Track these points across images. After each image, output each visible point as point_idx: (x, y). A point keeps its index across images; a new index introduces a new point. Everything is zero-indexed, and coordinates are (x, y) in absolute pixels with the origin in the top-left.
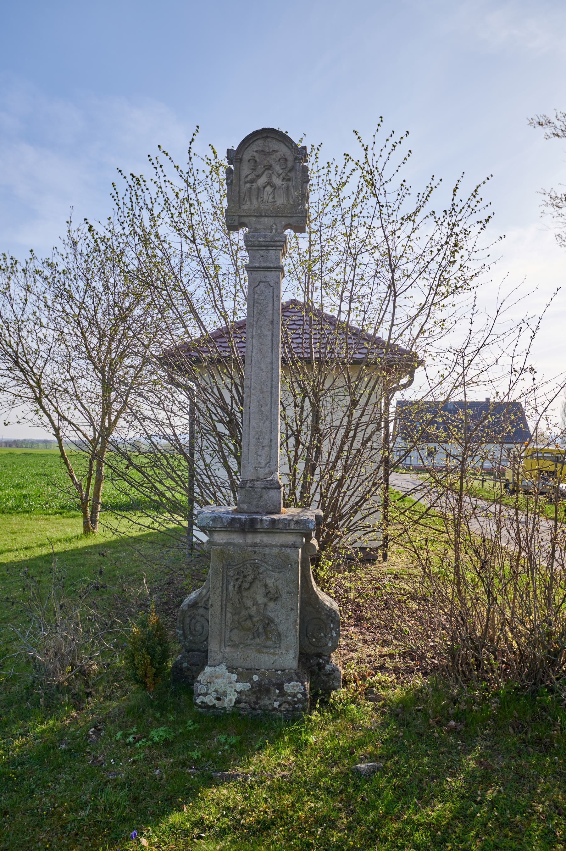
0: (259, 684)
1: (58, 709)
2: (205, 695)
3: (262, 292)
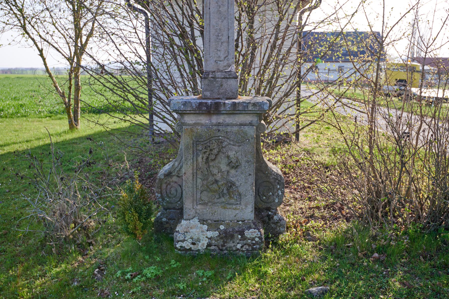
0: (225, 231)
1: (67, 255)
2: (183, 241)
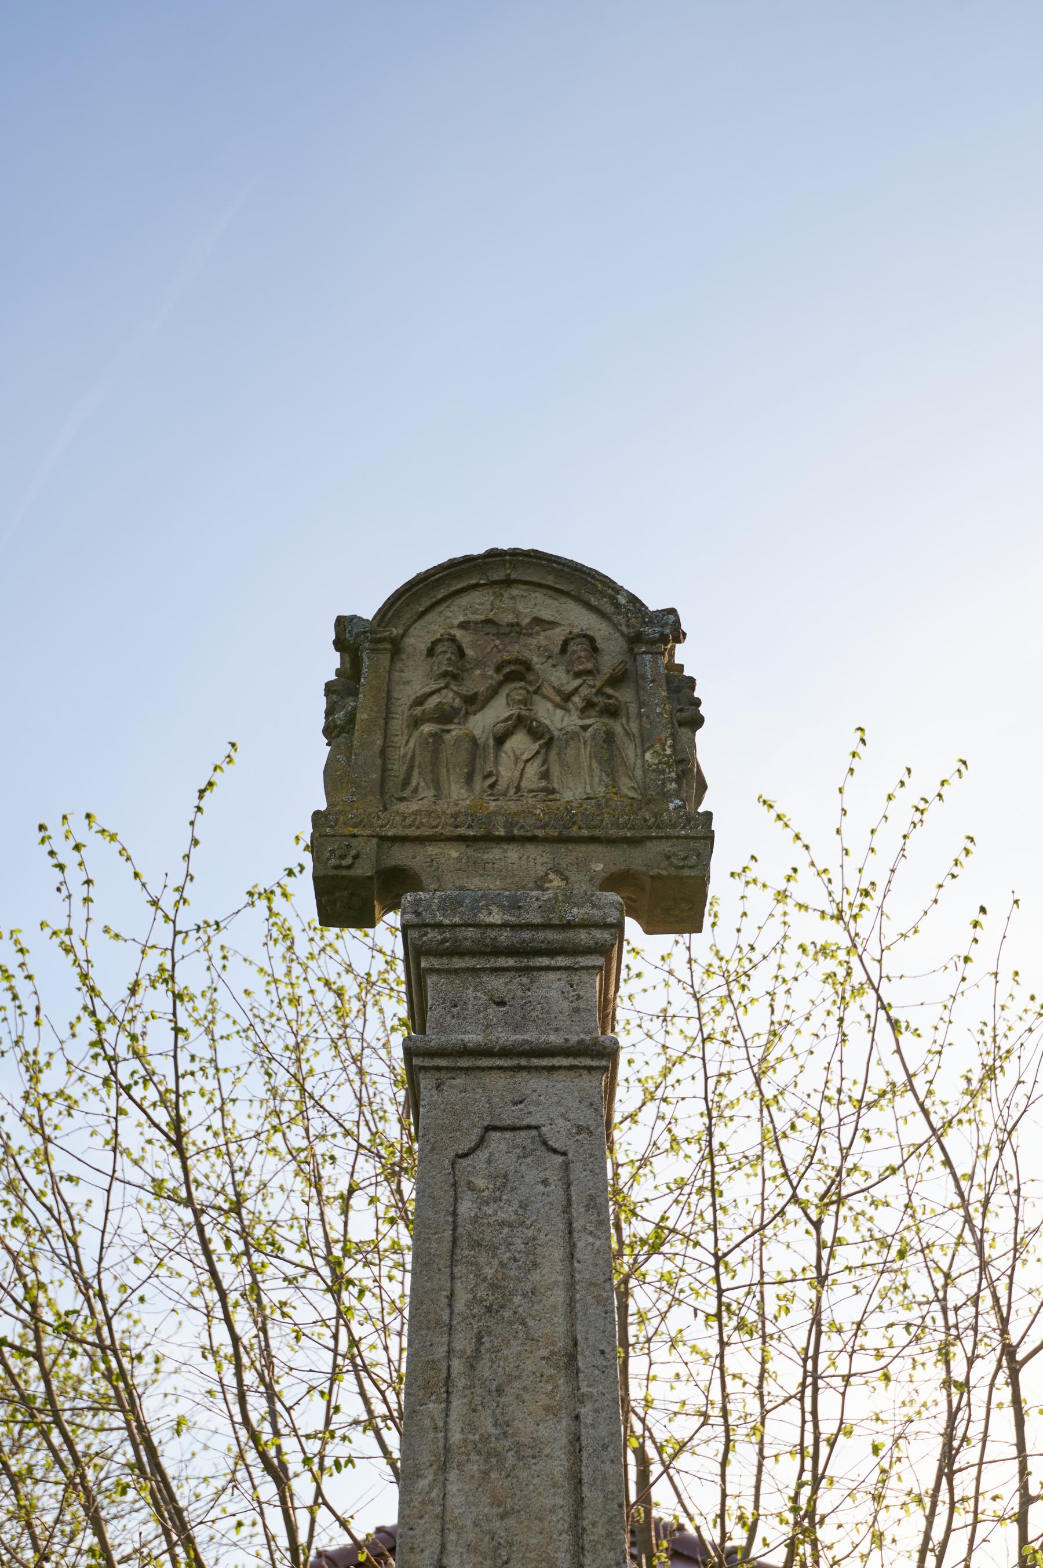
3: (503, 1181)
